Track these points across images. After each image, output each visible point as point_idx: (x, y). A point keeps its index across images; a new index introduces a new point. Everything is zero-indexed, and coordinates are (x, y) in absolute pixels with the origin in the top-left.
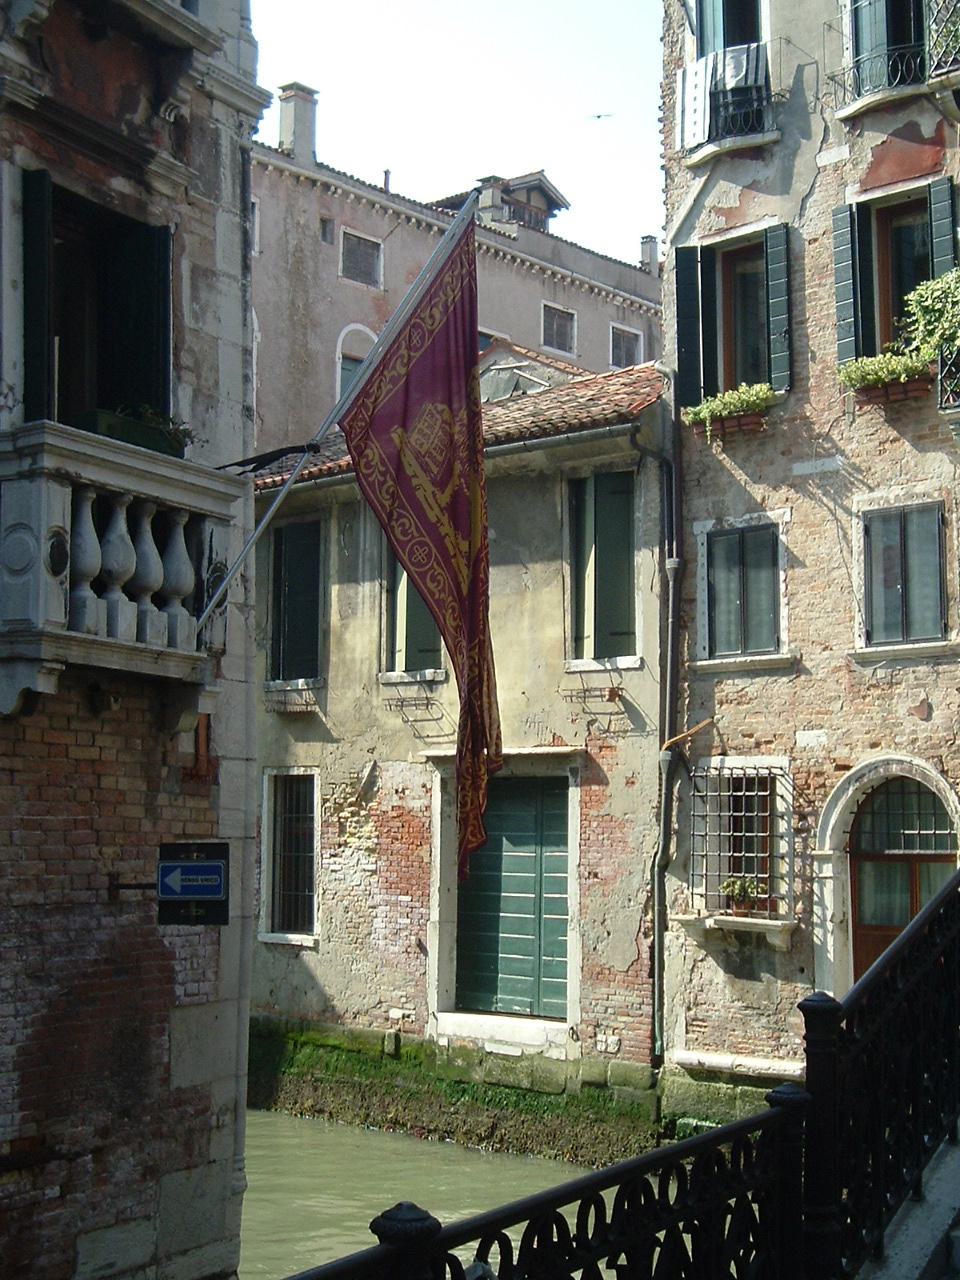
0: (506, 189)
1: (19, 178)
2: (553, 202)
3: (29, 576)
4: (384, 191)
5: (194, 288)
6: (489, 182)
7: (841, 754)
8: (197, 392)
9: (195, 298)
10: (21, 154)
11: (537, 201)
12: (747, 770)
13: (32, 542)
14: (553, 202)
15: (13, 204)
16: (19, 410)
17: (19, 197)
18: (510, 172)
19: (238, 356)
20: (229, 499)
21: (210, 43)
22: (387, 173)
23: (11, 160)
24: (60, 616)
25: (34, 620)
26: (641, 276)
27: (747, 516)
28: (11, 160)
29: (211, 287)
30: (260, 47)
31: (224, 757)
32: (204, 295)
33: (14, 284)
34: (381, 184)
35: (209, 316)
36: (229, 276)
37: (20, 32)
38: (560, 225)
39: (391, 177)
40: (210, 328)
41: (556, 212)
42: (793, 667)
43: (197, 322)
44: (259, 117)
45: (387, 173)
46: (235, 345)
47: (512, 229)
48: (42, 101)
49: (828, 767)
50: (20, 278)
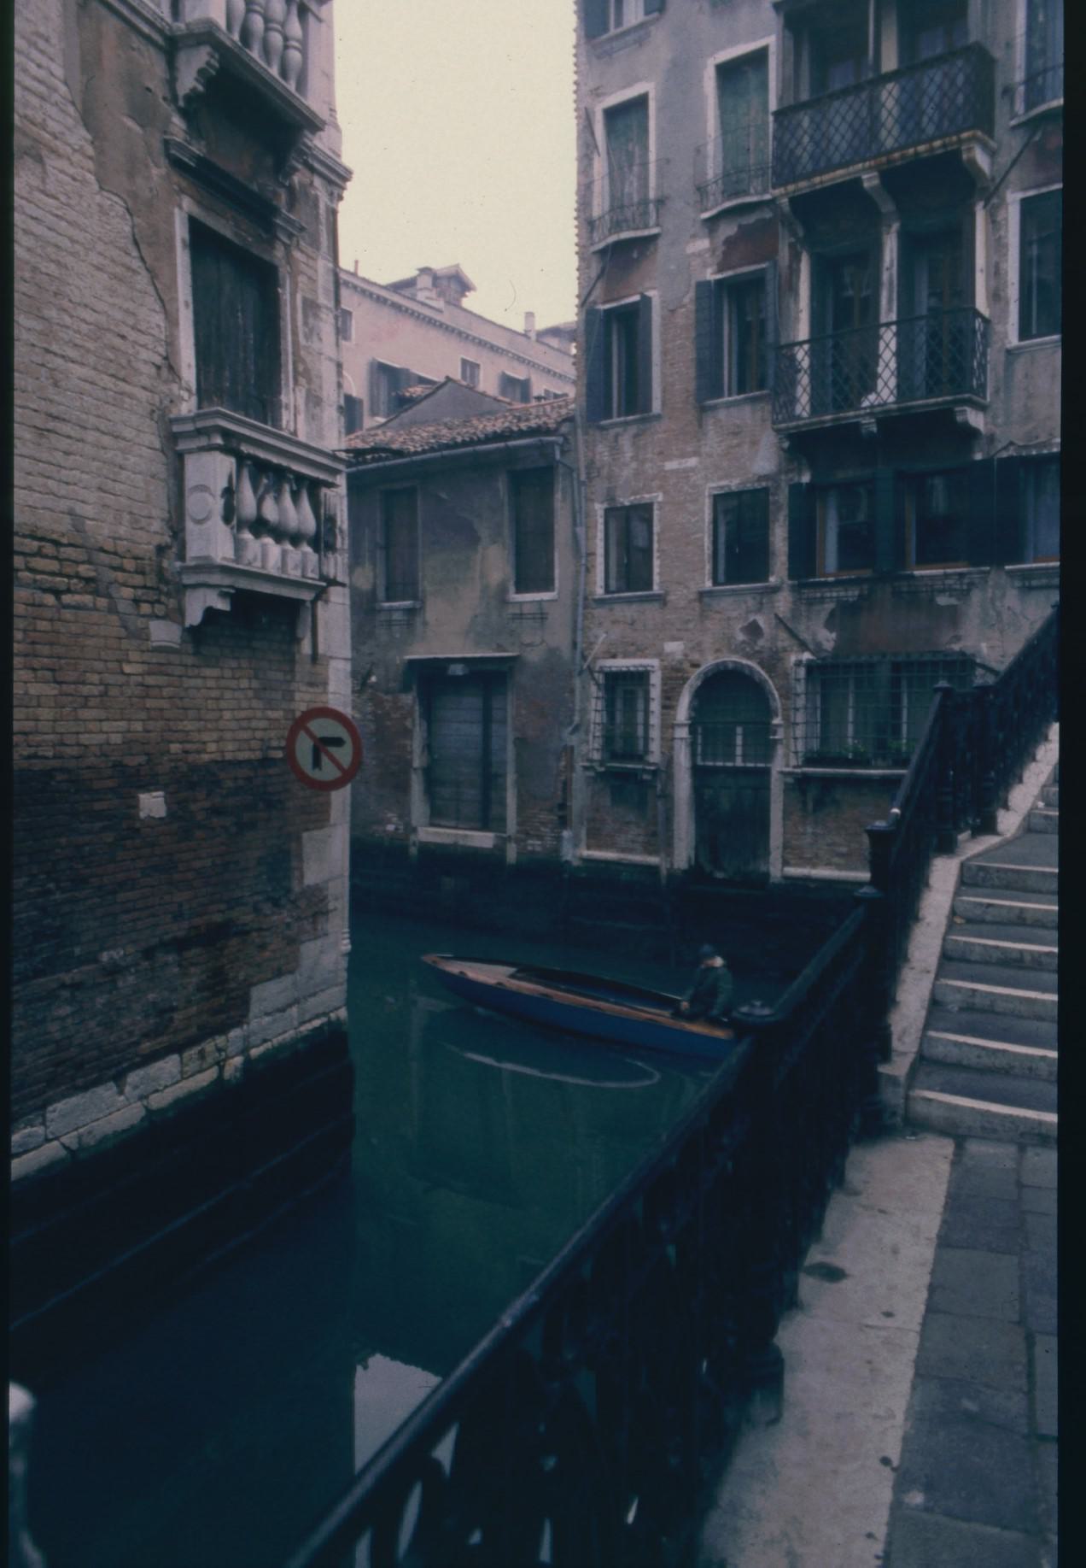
0: (436, 278)
1: (186, 221)
2: (464, 286)
3: (209, 523)
4: (354, 275)
5: (305, 316)
6: (425, 271)
7: (695, 657)
8: (309, 392)
9: (306, 323)
10: (187, 203)
11: (454, 286)
12: (226, 754)
13: (210, 499)
14: (464, 286)
15: (183, 241)
16: (194, 400)
17: (187, 236)
18: (439, 264)
19: (333, 368)
20: (335, 472)
21: (314, 125)
22: (356, 262)
23: (180, 207)
24: (230, 554)
25: (213, 555)
26: (523, 339)
27: (632, 498)
28: (180, 207)
29: (316, 316)
30: (343, 133)
31: (331, 658)
32: (311, 320)
33: (187, 304)
34: (352, 270)
35: (315, 338)
36: (328, 308)
37: (181, 103)
38: (469, 302)
39: (360, 265)
40: (316, 345)
41: (467, 294)
42: (661, 599)
43: (307, 341)
44: (343, 188)
45: (356, 262)
46: (331, 359)
47: (440, 304)
48: (199, 160)
49: (686, 666)
50: (190, 299)
